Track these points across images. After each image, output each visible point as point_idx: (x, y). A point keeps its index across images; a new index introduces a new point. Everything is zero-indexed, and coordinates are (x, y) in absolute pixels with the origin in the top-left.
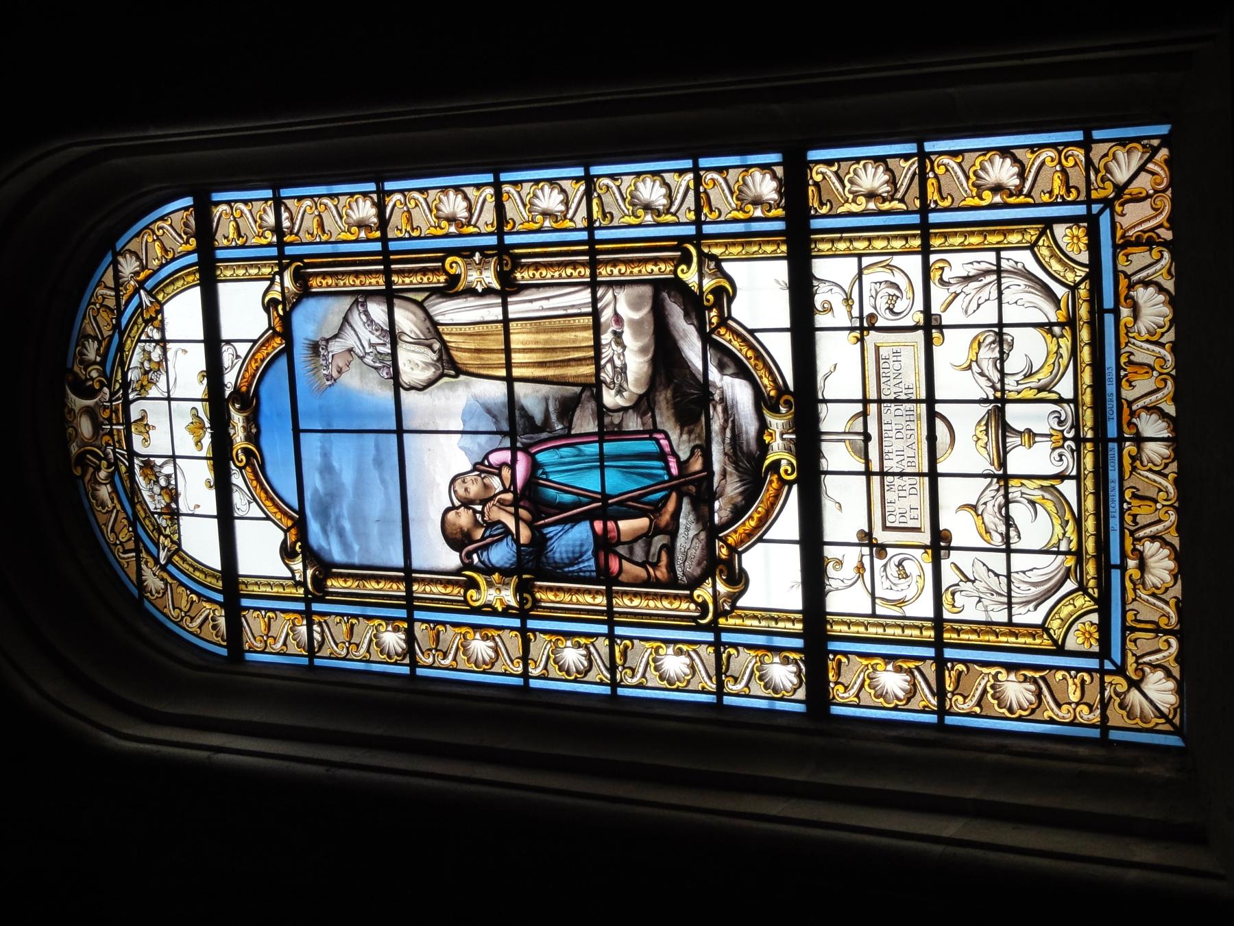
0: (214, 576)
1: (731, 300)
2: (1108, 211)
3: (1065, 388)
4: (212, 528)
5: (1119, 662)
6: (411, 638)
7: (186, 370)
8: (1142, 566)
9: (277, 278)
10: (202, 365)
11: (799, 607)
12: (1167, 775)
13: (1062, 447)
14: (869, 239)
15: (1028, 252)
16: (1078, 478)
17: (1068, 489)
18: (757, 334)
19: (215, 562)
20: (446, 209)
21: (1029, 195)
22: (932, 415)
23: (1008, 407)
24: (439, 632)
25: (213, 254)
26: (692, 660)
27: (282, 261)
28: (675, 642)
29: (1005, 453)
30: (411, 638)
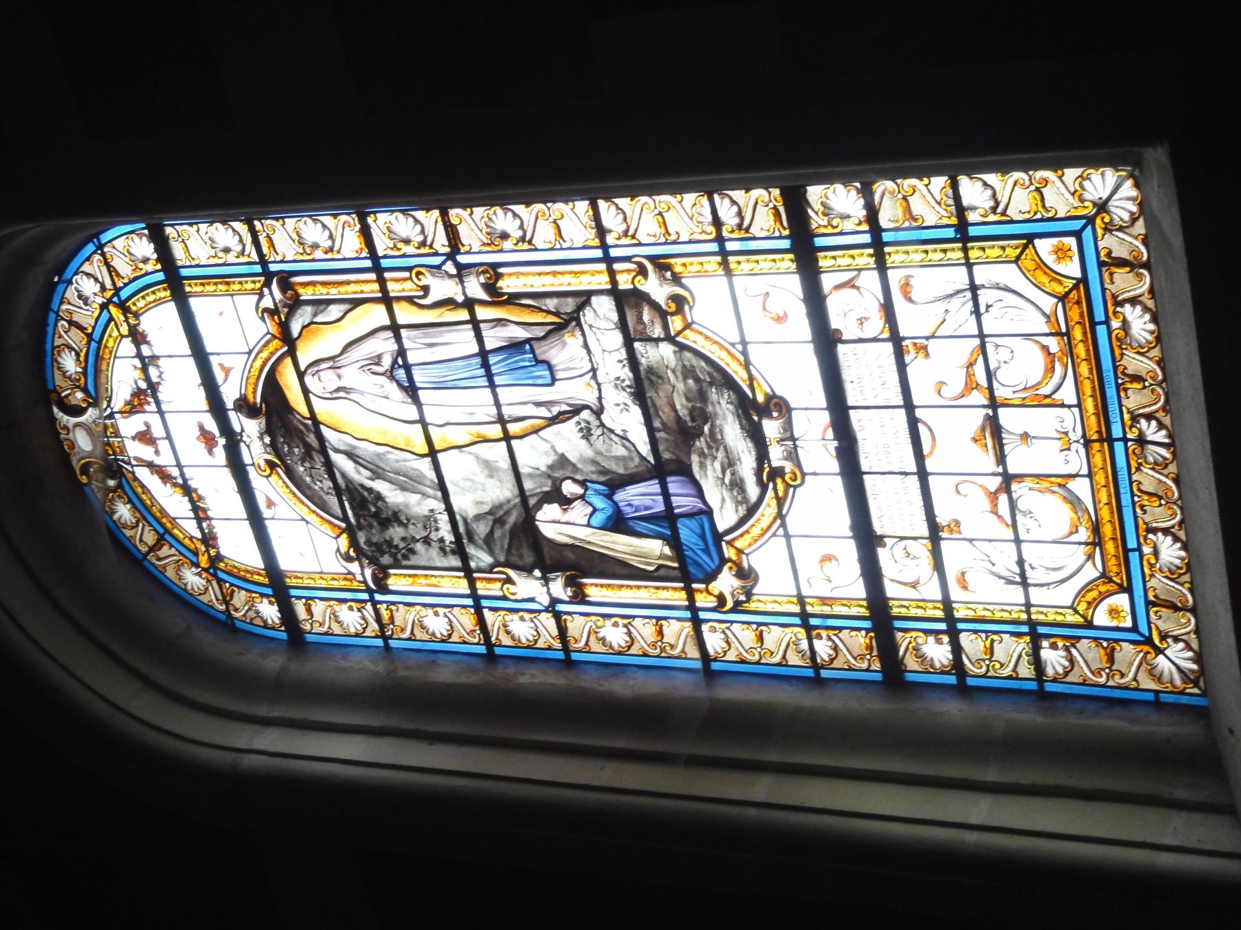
0: (259, 574)
1: (691, 308)
2: (1089, 228)
3: (1068, 394)
4: (246, 529)
5: (1147, 634)
6: (957, 649)
7: (180, 385)
8: (1156, 553)
9: (266, 290)
10: (197, 379)
11: (864, 595)
12: (373, 667)
13: (1069, 449)
14: (945, 251)
15: (1014, 265)
16: (1090, 475)
17: (1081, 488)
18: (303, 369)
19: (257, 562)
20: (221, 243)
21: (1004, 213)
22: (913, 423)
23: (1000, 410)
24: (762, 632)
25: (178, 273)
26: (833, 642)
27: (268, 276)
28: (610, 616)
29: (356, 462)
30: (957, 649)
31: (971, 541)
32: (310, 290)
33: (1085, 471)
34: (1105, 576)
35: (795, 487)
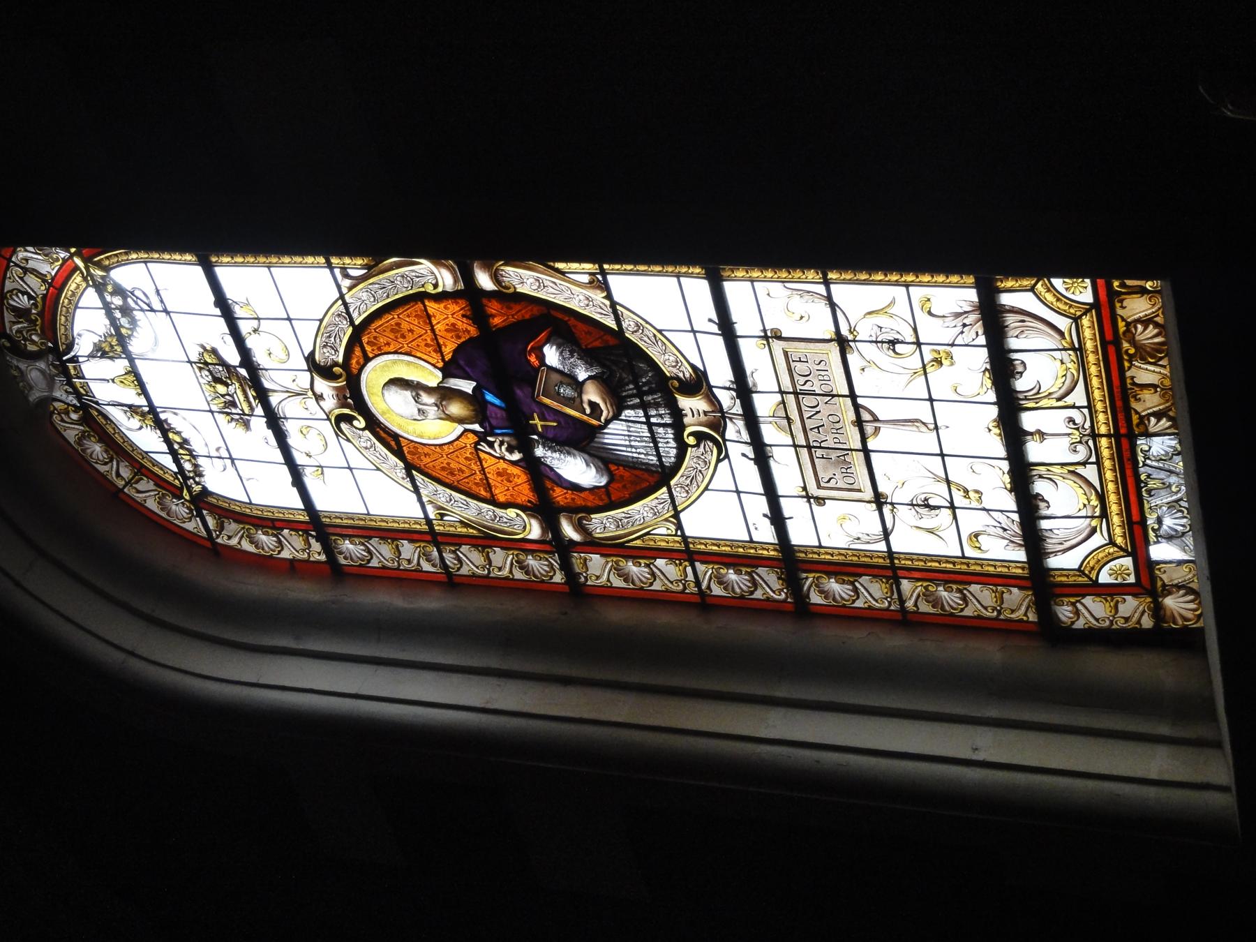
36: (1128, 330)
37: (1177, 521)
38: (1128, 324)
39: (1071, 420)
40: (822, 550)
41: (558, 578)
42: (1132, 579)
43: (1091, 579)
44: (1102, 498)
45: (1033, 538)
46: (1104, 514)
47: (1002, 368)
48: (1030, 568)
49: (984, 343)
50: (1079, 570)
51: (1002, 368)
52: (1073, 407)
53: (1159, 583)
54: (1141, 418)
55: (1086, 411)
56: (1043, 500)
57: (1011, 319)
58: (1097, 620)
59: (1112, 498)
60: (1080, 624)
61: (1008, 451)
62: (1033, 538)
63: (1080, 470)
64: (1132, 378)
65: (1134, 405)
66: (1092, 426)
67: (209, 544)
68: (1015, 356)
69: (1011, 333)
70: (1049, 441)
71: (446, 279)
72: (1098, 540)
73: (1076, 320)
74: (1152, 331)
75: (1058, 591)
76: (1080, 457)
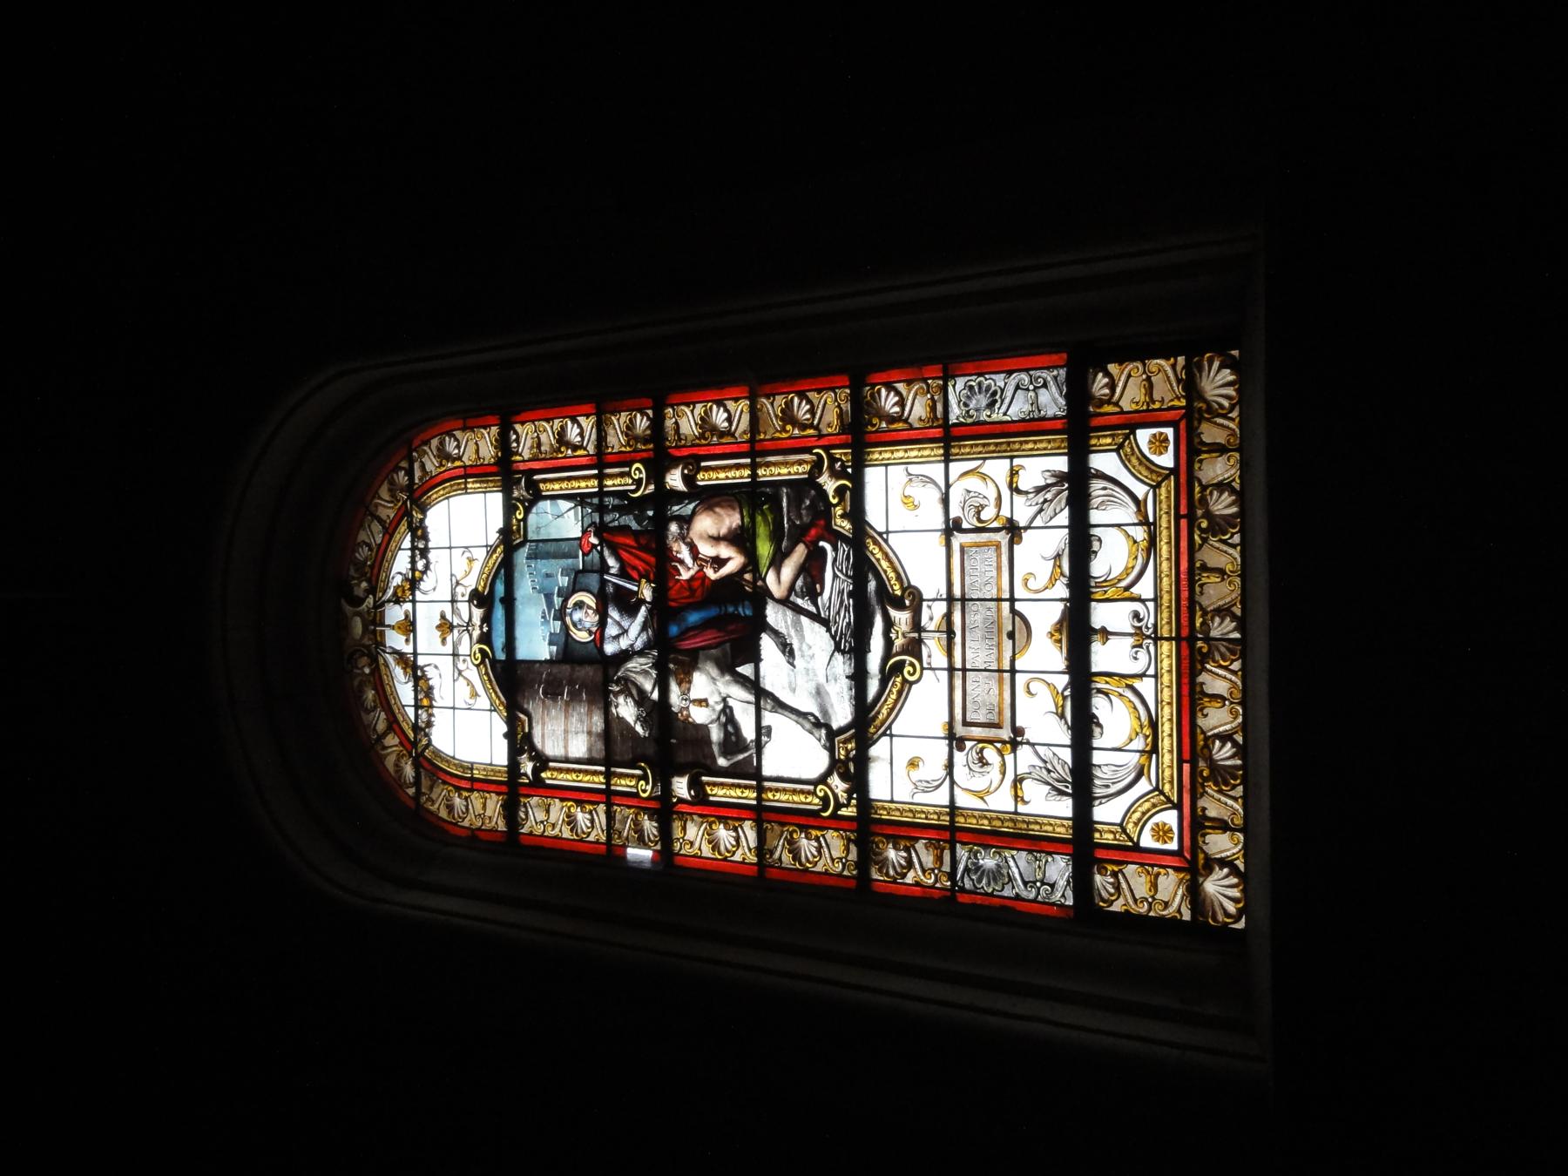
3: (1145, 588)
31: (1033, 745)
32: (549, 486)
33: (1151, 671)
34: (1158, 789)
35: (911, 683)
36: (1206, 746)
37: (1222, 890)
38: (1206, 739)
39: (1136, 616)
40: (893, 806)
41: (655, 696)
42: (1169, 432)
43: (1131, 839)
44: (1154, 725)
45: (1081, 782)
46: (1155, 749)
47: (1081, 544)
48: (1074, 827)
49: (1066, 522)
50: (1117, 451)
51: (1081, 544)
52: (1139, 599)
53: (1201, 856)
54: (1206, 739)
55: (1151, 605)
56: (1100, 726)
57: (1097, 487)
58: (1135, 900)
59: (1166, 728)
60: (1117, 907)
61: (1071, 593)
62: (1081, 782)
63: (1137, 684)
64: (1204, 809)
65: (1201, 721)
66: (1155, 625)
67: (412, 804)
68: (1095, 531)
69: (1095, 502)
70: (1113, 641)
71: (646, 789)
72: (1143, 786)
73: (1156, 487)
74: (1228, 749)
75: (1100, 854)
76: (1137, 668)
